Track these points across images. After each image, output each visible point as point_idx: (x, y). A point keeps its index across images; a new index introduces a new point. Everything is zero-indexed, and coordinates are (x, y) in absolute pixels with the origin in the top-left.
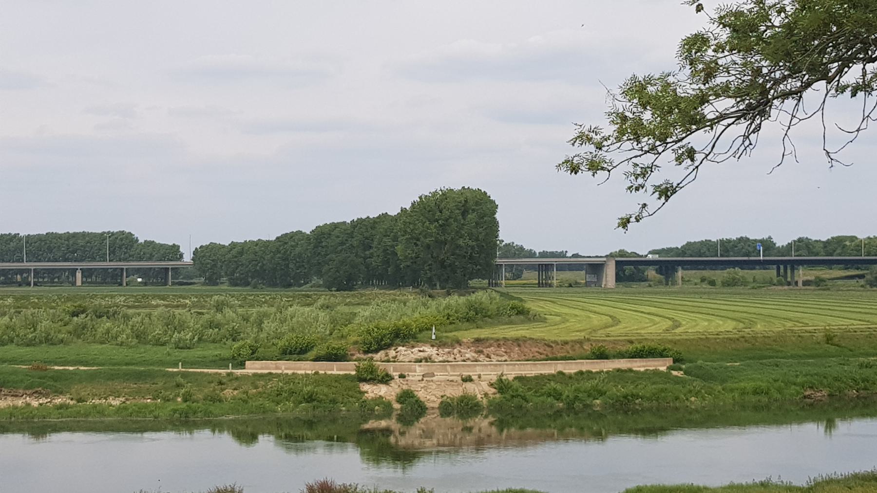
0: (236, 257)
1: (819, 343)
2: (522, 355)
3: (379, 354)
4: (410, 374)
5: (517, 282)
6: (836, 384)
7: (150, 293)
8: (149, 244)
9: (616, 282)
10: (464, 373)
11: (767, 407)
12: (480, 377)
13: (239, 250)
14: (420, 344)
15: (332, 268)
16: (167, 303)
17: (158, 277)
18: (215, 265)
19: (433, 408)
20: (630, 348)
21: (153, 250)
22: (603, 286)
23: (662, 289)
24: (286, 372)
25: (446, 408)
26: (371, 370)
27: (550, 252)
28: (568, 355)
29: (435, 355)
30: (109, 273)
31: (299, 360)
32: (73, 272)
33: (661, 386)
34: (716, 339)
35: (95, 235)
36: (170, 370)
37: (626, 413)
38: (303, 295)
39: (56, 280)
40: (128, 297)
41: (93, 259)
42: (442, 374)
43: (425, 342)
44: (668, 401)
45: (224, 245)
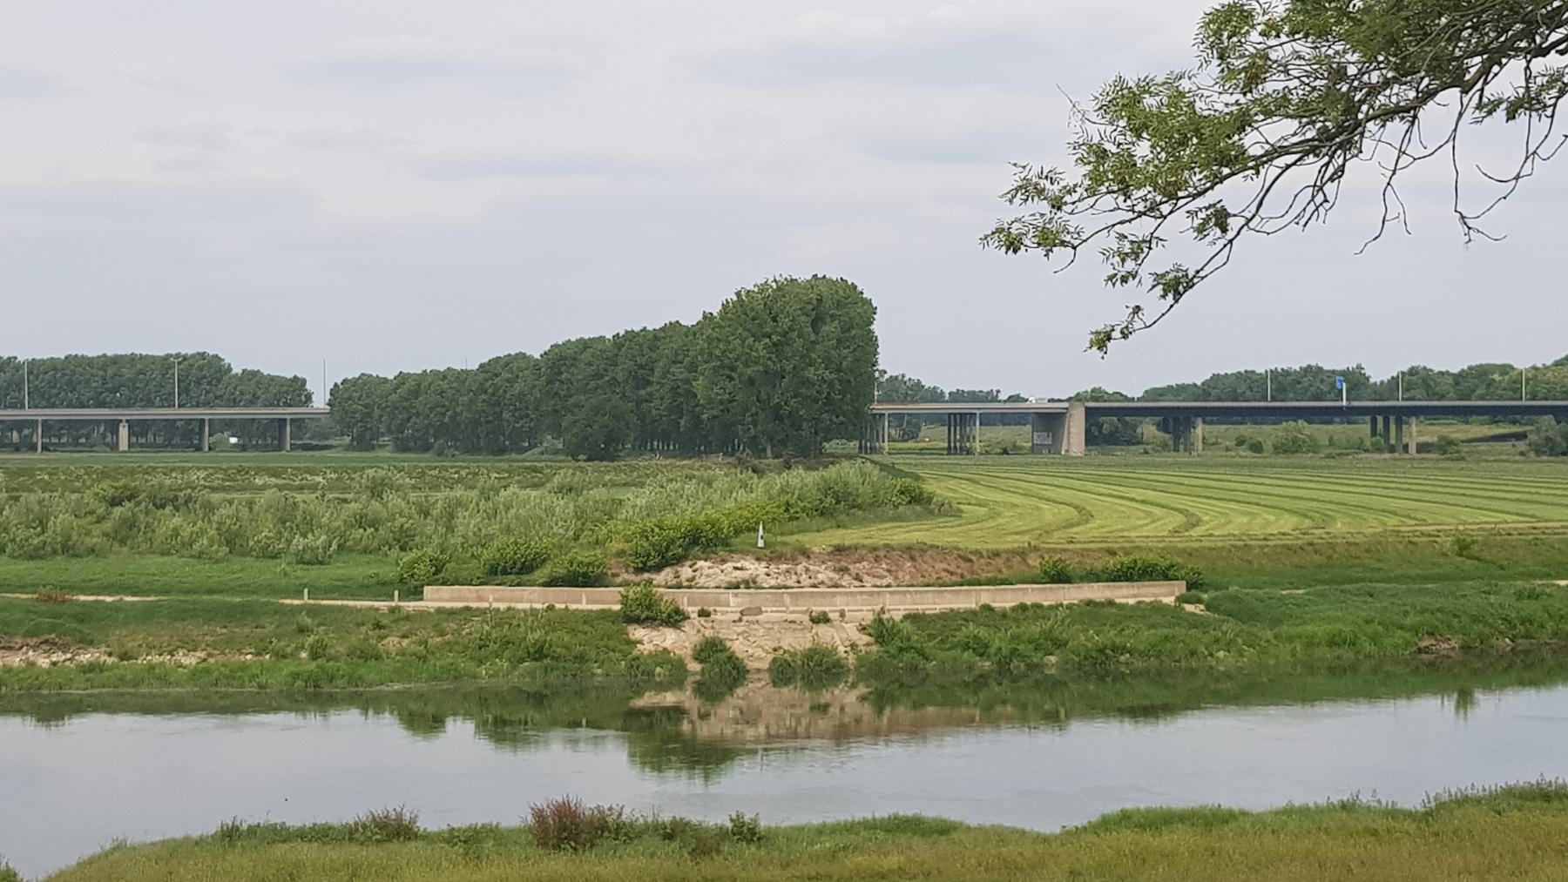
0: (406, 399)
3: (663, 573)
4: (718, 609)
5: (911, 444)
9: (1086, 445)
10: (814, 608)
11: (1353, 669)
12: (842, 614)
13: (412, 388)
14: (735, 556)
17: (266, 436)
18: (369, 415)
19: (758, 671)
20: (1112, 562)
21: (257, 386)
22: (1063, 453)
23: (1169, 457)
24: (495, 605)
25: (782, 671)
27: (968, 392)
28: (1000, 576)
29: (763, 576)
32: (113, 426)
34: (1262, 547)
37: (1102, 678)
38: (526, 468)
39: (83, 440)
40: (211, 471)
41: (150, 403)
42: (774, 609)
43: (745, 553)
44: (1177, 658)
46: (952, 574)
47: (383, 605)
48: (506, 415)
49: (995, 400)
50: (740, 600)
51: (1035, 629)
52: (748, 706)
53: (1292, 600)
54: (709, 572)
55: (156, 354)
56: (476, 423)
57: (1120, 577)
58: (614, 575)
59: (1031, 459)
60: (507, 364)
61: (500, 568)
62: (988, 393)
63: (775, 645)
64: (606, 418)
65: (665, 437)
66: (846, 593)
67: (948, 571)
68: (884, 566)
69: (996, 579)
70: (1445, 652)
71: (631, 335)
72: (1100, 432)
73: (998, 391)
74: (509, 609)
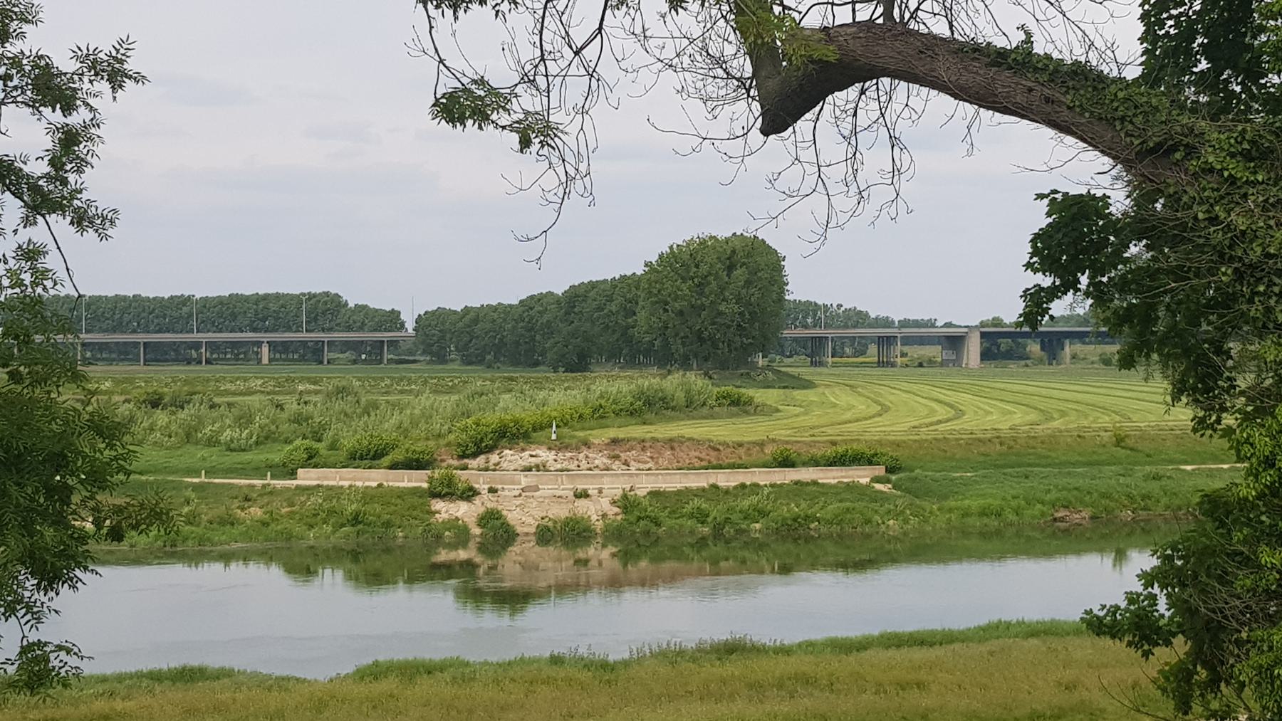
0: (469, 326)
1: (1104, 446)
2: (675, 461)
3: (478, 459)
4: (505, 487)
5: (861, 359)
6: (1103, 502)
7: (298, 375)
8: (361, 308)
9: (982, 360)
10: (579, 487)
11: (998, 533)
12: (600, 491)
13: (473, 317)
14: (532, 446)
15: (559, 342)
16: (319, 388)
18: (443, 338)
19: (527, 534)
20: (830, 451)
22: (964, 366)
23: (1046, 369)
24: (341, 483)
25: (545, 535)
26: (449, 482)
27: (913, 321)
28: (740, 462)
29: (551, 461)
30: (308, 347)
31: (370, 468)
32: (259, 344)
33: (848, 504)
34: (957, 439)
35: (292, 297)
36: (189, 480)
37: (795, 540)
38: (505, 378)
39: (242, 356)
40: (266, 379)
41: (289, 329)
42: (550, 487)
43: (541, 443)
44: (855, 525)
45: (455, 311)
46: (702, 460)
47: (258, 482)
48: (538, 337)
49: (933, 326)
50: (529, 480)
51: (745, 504)
52: (526, 561)
53: (961, 481)
54: (511, 458)
55: (294, 293)
56: (517, 343)
57: (835, 462)
58: (443, 461)
59: (943, 370)
60: (539, 300)
61: (358, 454)
62: (928, 321)
63: (544, 514)
64: (578, 340)
65: (647, 354)
66: (612, 475)
67: (699, 458)
68: (649, 454)
69: (734, 464)
70: (1077, 521)
71: (623, 277)
72: (998, 350)
73: (935, 320)
74: (350, 486)
